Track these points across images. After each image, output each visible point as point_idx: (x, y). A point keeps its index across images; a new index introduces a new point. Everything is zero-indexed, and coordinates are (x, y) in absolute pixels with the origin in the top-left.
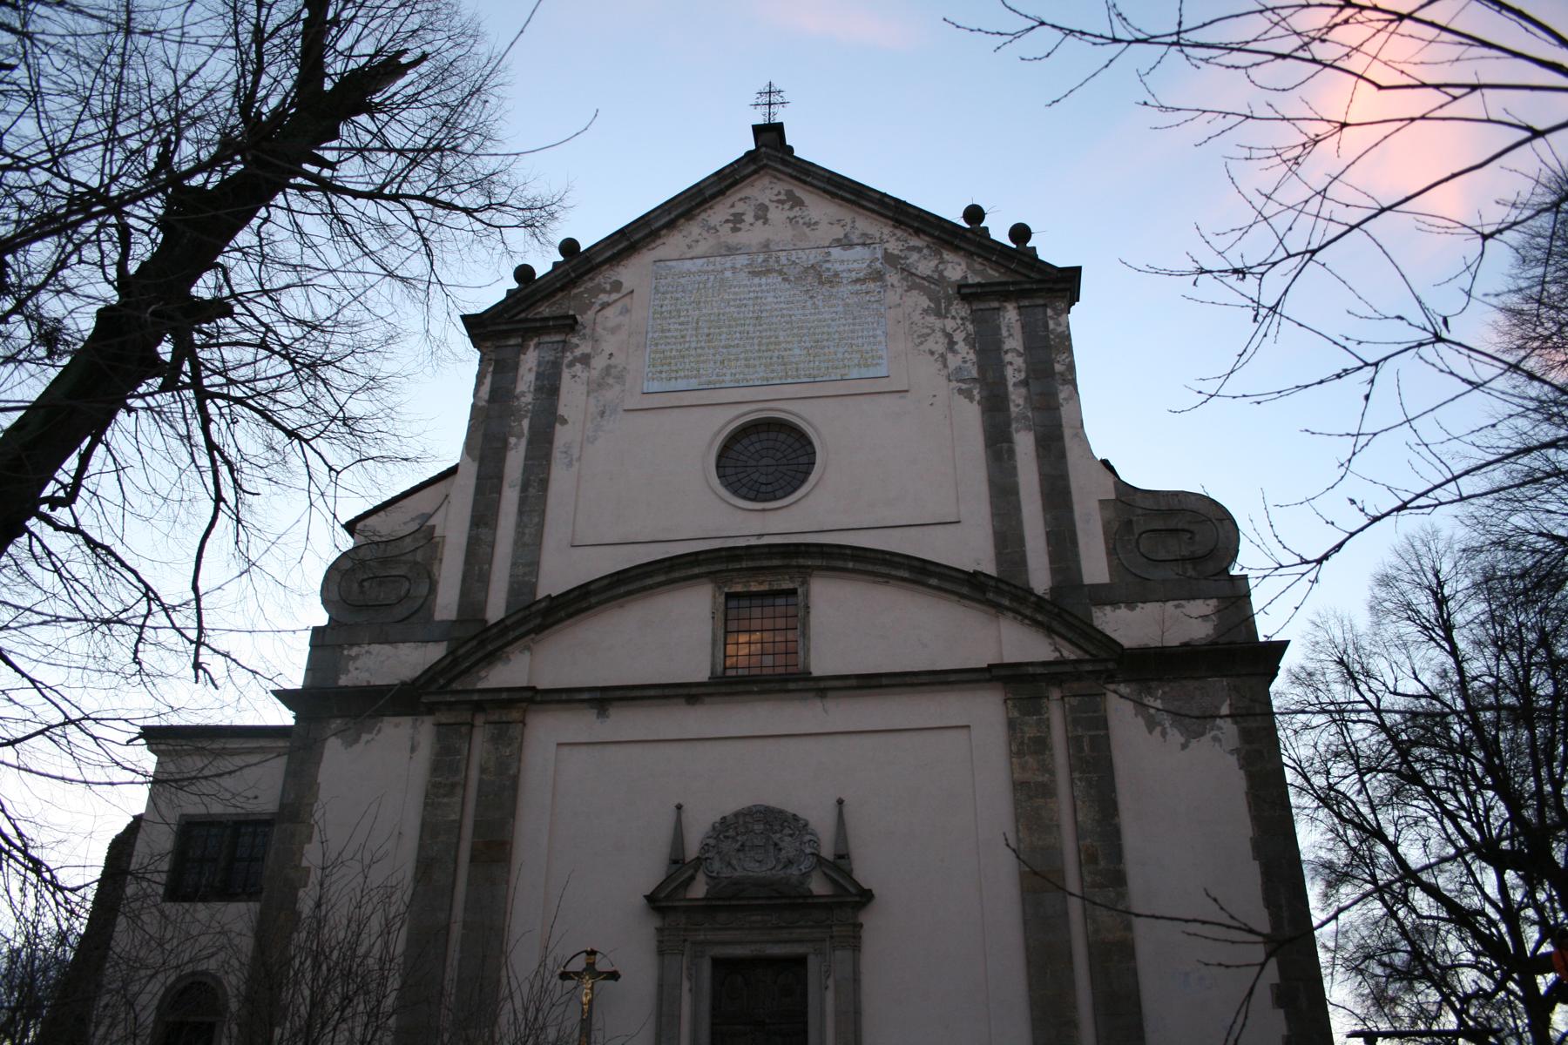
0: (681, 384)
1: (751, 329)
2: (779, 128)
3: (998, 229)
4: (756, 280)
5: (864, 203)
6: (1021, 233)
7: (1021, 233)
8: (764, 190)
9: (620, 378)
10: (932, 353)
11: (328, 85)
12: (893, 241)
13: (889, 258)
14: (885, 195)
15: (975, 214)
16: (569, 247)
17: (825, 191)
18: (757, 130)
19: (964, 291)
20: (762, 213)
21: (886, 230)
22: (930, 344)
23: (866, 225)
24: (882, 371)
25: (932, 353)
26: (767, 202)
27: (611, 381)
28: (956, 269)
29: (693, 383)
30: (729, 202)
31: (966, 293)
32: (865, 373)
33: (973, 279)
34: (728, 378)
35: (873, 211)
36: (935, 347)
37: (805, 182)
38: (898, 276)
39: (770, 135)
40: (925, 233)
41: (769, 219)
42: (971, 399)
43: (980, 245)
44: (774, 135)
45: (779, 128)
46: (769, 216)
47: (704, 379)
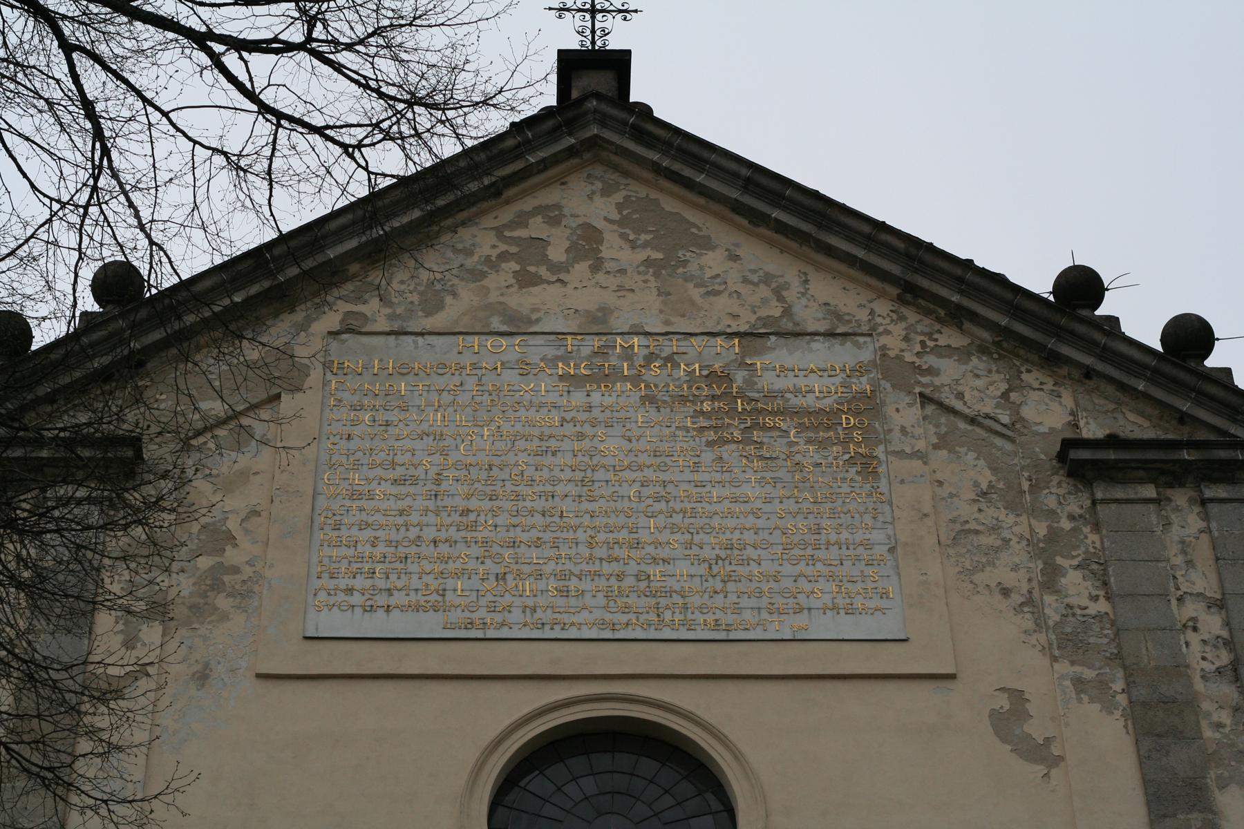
0: (399, 624)
1: (567, 506)
2: (620, 62)
3: (1141, 317)
4: (578, 398)
5: (834, 241)
6: (1191, 336)
7: (1191, 336)
8: (587, 201)
9: (244, 595)
10: (1006, 592)
11: (1051, 298)
12: (898, 331)
13: (887, 365)
14: (882, 226)
15: (1081, 286)
16: (117, 283)
17: (738, 208)
18: (569, 63)
19: (1075, 454)
20: (587, 243)
21: (883, 308)
22: (1001, 573)
23: (820, 293)
24: (888, 626)
25: (1006, 592)
26: (600, 224)
27: (223, 602)
28: (1050, 410)
29: (430, 625)
30: (507, 214)
31: (1081, 463)
32: (847, 627)
33: (1092, 430)
34: (516, 616)
35: (851, 260)
36: (1010, 579)
37: (688, 184)
38: (916, 411)
39: (593, 75)
40: (974, 317)
41: (594, 253)
42: (1109, 707)
43: (1106, 354)
44: (601, 81)
45: (620, 62)
46: (606, 253)
47: (456, 616)
